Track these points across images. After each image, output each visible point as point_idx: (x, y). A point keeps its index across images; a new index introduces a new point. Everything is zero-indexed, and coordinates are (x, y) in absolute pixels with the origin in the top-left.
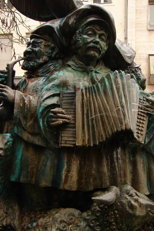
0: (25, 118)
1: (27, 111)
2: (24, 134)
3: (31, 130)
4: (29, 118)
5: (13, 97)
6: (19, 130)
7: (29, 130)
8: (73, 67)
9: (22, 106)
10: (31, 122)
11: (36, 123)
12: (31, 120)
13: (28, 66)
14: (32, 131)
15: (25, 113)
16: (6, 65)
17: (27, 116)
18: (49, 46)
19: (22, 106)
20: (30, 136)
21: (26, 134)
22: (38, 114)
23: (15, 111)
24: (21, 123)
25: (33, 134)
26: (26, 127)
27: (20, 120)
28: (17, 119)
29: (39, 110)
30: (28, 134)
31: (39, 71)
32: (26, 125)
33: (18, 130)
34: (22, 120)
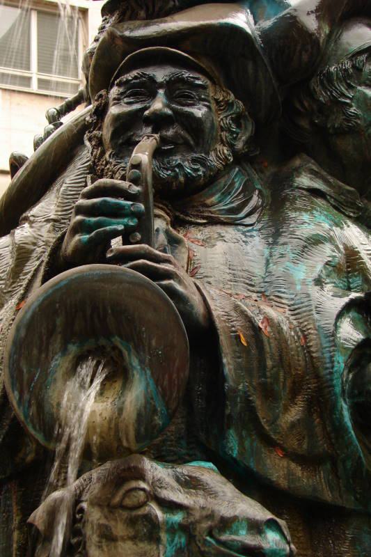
0: (269, 393)
1: (274, 367)
2: (268, 461)
3: (300, 445)
4: (284, 394)
5: (352, 314)
6: (247, 443)
7: (292, 443)
8: (332, 201)
9: (247, 342)
10: (294, 413)
11: (315, 416)
12: (292, 400)
13: (176, 176)
14: (305, 446)
15: (268, 374)
16: (9, 157)
17: (276, 388)
18: (229, 105)
19: (245, 344)
20: (298, 470)
21: (277, 461)
22: (332, 380)
23: (228, 363)
24: (257, 416)
25: (308, 461)
26: (275, 433)
27: (248, 403)
28: (239, 399)
29: (332, 362)
30: (285, 463)
31: (208, 202)
32: (273, 422)
33: (241, 444)
34: (257, 402)
